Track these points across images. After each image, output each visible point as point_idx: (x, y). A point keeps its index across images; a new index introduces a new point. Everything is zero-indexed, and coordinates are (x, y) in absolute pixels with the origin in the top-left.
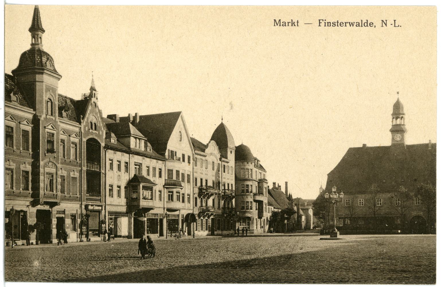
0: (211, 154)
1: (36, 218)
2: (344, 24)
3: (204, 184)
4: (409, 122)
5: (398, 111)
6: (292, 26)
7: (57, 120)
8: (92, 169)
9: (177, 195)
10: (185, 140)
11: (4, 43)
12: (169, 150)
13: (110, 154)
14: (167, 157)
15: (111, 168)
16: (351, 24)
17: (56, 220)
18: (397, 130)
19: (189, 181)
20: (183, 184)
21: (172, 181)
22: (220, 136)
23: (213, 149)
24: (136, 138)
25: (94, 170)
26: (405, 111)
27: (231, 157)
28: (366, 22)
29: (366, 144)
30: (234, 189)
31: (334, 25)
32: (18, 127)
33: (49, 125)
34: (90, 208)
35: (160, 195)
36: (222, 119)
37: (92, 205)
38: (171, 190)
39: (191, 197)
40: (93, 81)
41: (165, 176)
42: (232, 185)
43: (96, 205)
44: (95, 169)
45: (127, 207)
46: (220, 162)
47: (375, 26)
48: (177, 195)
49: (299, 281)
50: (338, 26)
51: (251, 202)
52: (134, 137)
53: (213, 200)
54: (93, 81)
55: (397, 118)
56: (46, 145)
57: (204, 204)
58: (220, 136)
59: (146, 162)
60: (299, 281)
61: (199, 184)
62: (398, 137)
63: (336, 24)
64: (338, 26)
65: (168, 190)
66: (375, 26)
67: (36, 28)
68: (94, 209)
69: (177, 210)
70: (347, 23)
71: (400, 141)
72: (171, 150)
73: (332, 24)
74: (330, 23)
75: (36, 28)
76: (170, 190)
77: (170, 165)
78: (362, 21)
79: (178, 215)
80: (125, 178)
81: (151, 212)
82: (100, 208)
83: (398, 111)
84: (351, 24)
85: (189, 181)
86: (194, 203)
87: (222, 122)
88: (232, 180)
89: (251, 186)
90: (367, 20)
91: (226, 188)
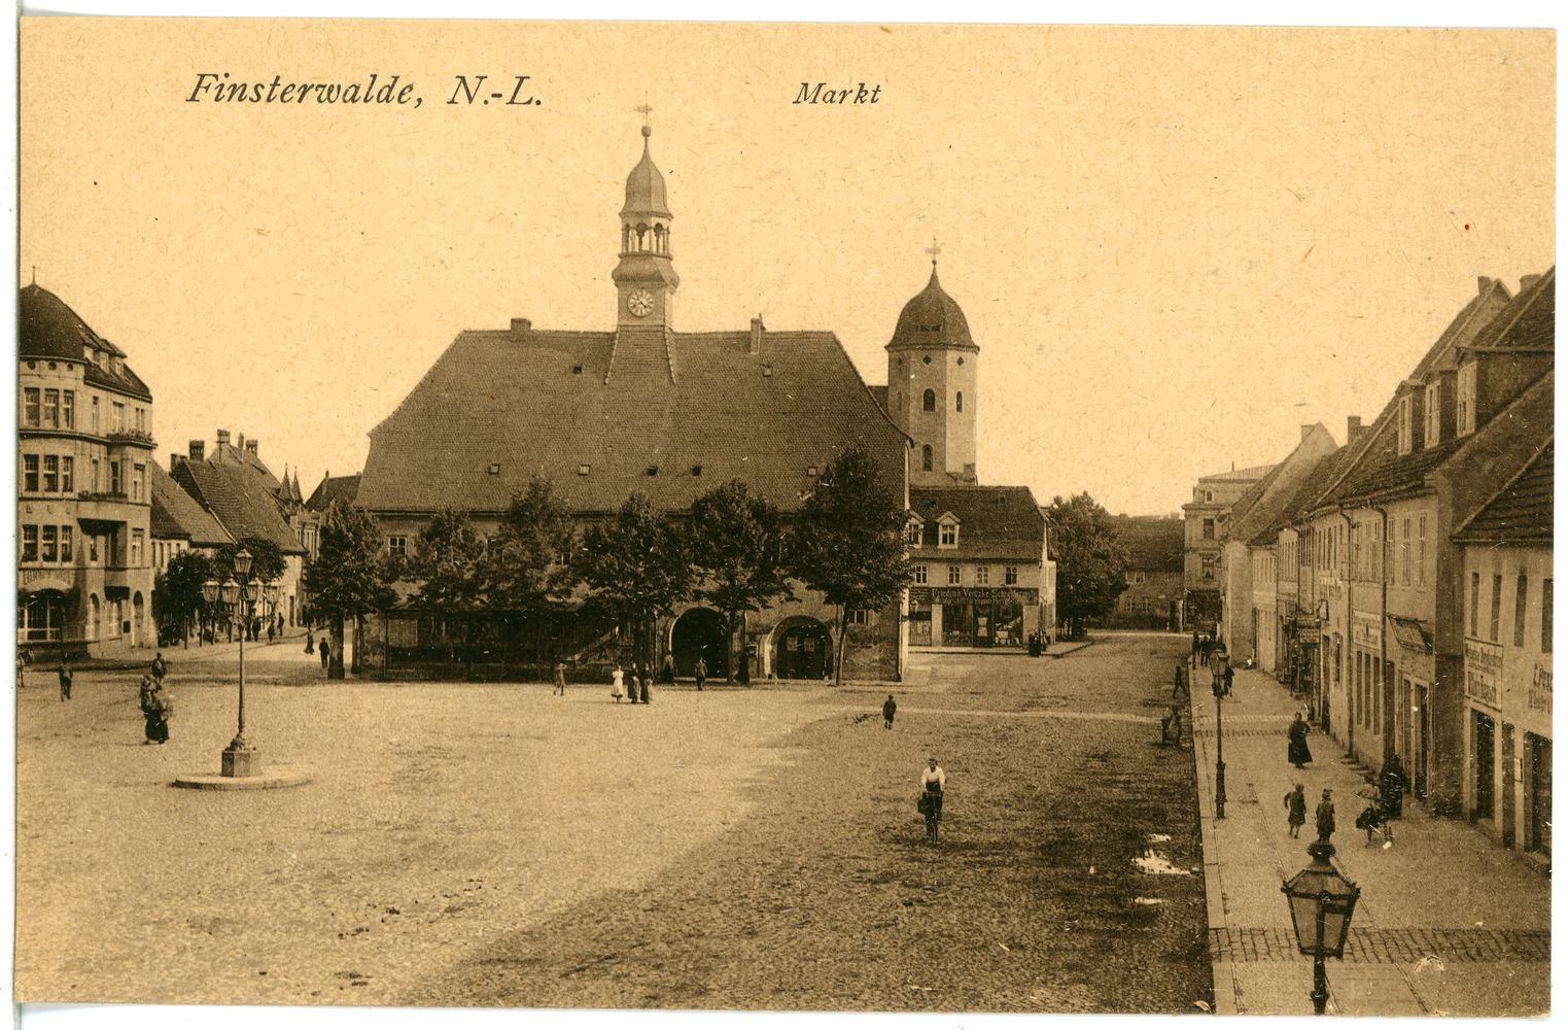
5: (643, 206)
16: (327, 93)
18: (642, 275)
26: (674, 203)
27: (74, 556)
29: (161, 742)
47: (420, 100)
49: (1118, 646)
51: (66, 528)
55: (641, 230)
60: (1118, 646)
62: (643, 299)
66: (420, 100)
83: (643, 206)
84: (327, 93)
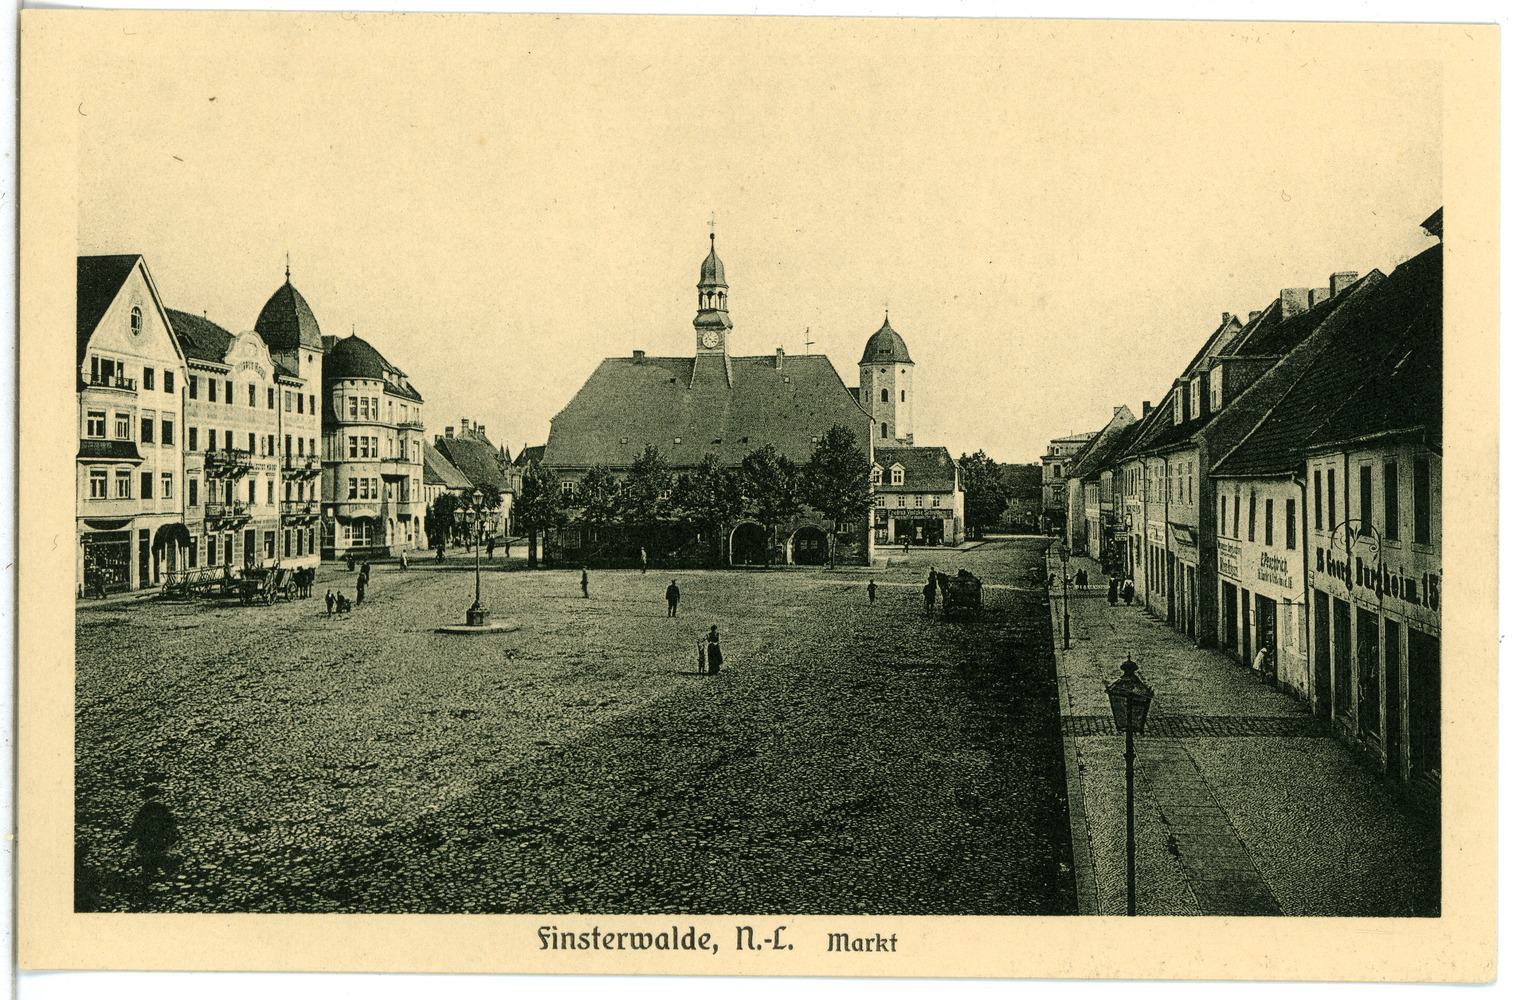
0: (246, 365)
2: (616, 938)
3: (221, 444)
4: (737, 306)
10: (156, 329)
18: (710, 322)
19: (167, 438)
21: (103, 445)
22: (282, 321)
27: (310, 371)
28: (689, 931)
31: (584, 945)
36: (288, 274)
38: (99, 468)
42: (312, 441)
46: (275, 387)
48: (121, 482)
50: (596, 947)
53: (252, 485)
57: (221, 498)
58: (282, 321)
61: (203, 442)
62: (711, 338)
63: (591, 939)
64: (596, 947)
65: (88, 468)
66: (716, 947)
69: (128, 521)
70: (626, 935)
71: (716, 347)
73: (577, 941)
74: (572, 935)
76: (94, 469)
78: (675, 929)
86: (187, 493)
87: (288, 284)
90: (692, 929)
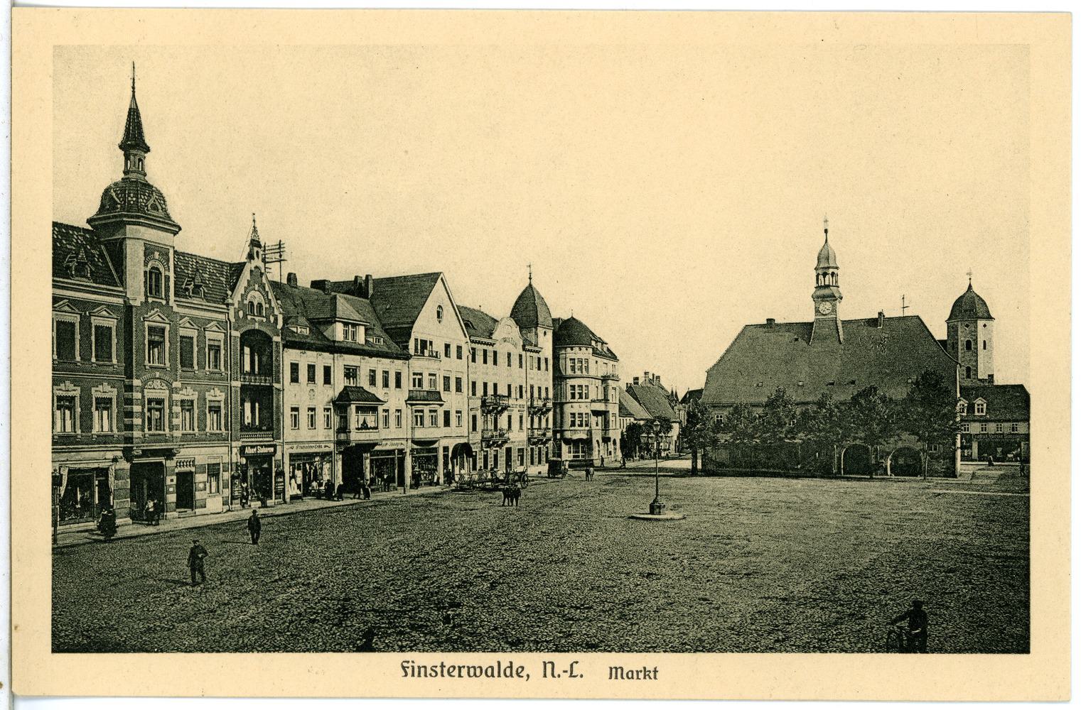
1: (130, 478)
3: (490, 391)
4: (845, 284)
6: (645, 678)
7: (172, 303)
8: (265, 383)
9: (432, 416)
11: (7, 155)
12: (416, 340)
13: (290, 356)
14: (412, 351)
15: (295, 379)
17: (174, 478)
18: (826, 294)
19: (459, 389)
20: (444, 395)
22: (527, 310)
23: (508, 332)
24: (346, 324)
25: (248, 383)
30: (551, 396)
32: (174, 331)
33: (1009, 421)
34: (249, 451)
35: (399, 418)
37: (252, 447)
39: (465, 414)
40: (255, 230)
41: (407, 384)
42: (547, 389)
43: (262, 446)
44: (265, 383)
45: (914, 327)
48: (432, 416)
52: (342, 322)
54: (255, 230)
56: (147, 351)
58: (527, 310)
59: (366, 365)
61: (480, 392)
62: (826, 307)
67: (134, 141)
68: (257, 453)
72: (421, 340)
75: (134, 141)
77: (417, 364)
79: (275, 499)
80: (324, 395)
81: (377, 448)
82: (272, 450)
85: (459, 389)
88: (546, 380)
89: (587, 386)
91: (536, 395)
